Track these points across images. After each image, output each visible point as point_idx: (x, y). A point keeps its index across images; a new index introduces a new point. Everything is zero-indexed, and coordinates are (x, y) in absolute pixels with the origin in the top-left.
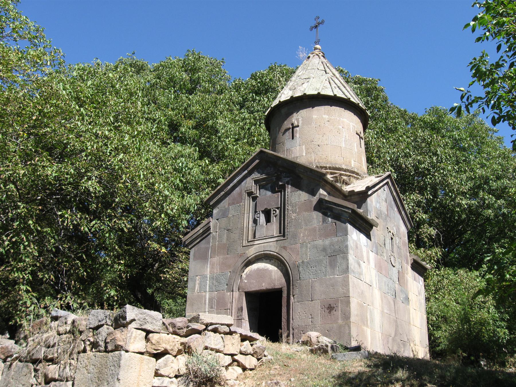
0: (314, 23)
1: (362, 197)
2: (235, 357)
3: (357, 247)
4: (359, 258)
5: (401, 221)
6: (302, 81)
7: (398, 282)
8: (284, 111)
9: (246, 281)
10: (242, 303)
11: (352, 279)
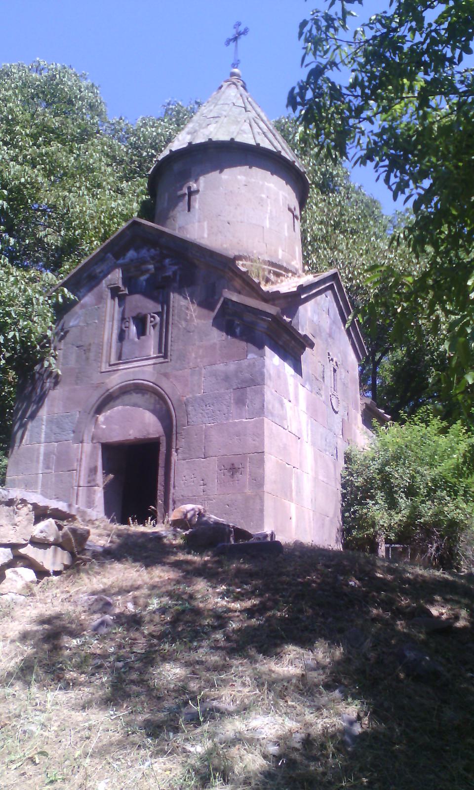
0: (231, 33)
1: (294, 300)
2: (22, 551)
3: (279, 377)
4: (282, 394)
5: (350, 348)
6: (207, 121)
7: (341, 436)
8: (177, 167)
9: (104, 427)
10: (96, 461)
11: (269, 425)
